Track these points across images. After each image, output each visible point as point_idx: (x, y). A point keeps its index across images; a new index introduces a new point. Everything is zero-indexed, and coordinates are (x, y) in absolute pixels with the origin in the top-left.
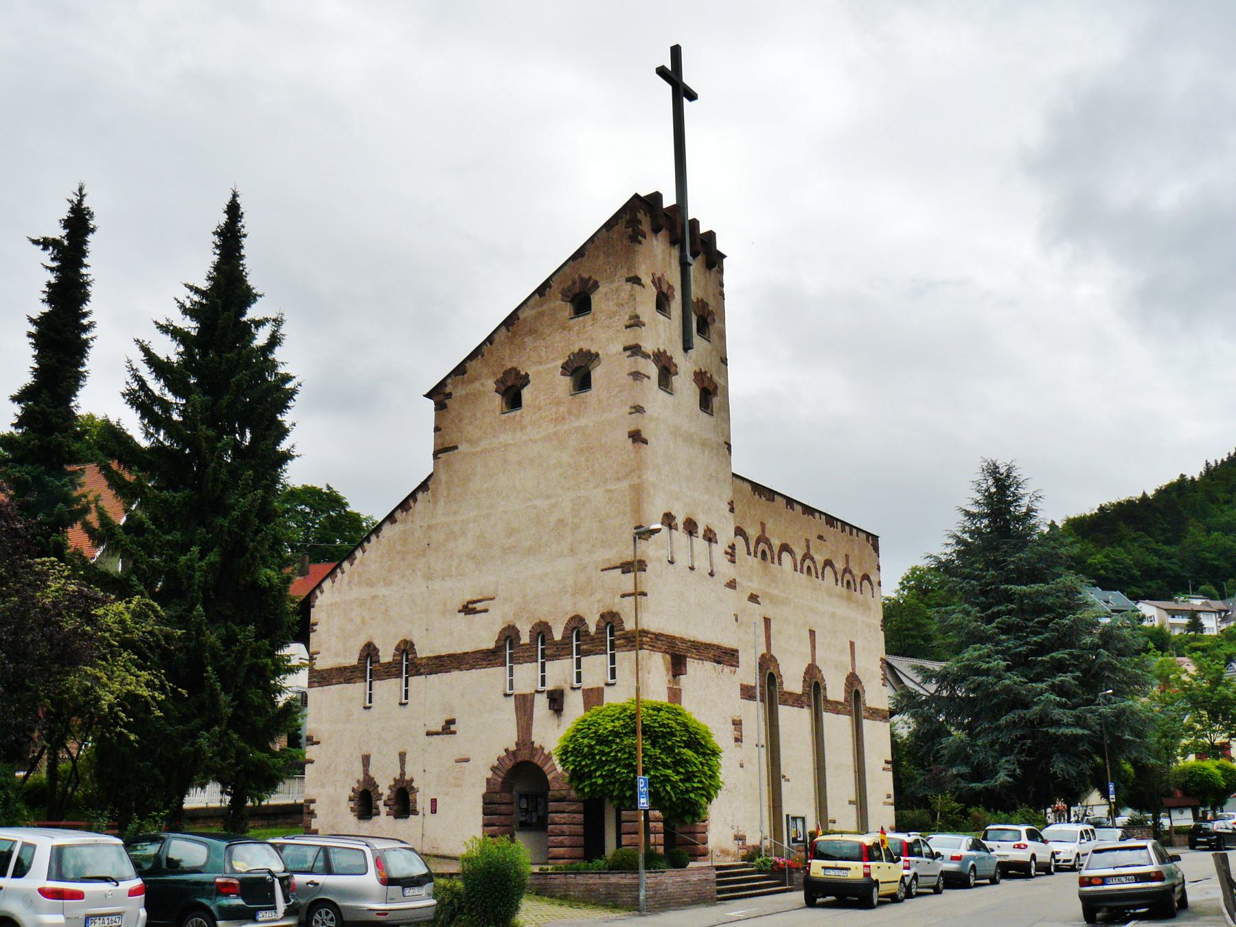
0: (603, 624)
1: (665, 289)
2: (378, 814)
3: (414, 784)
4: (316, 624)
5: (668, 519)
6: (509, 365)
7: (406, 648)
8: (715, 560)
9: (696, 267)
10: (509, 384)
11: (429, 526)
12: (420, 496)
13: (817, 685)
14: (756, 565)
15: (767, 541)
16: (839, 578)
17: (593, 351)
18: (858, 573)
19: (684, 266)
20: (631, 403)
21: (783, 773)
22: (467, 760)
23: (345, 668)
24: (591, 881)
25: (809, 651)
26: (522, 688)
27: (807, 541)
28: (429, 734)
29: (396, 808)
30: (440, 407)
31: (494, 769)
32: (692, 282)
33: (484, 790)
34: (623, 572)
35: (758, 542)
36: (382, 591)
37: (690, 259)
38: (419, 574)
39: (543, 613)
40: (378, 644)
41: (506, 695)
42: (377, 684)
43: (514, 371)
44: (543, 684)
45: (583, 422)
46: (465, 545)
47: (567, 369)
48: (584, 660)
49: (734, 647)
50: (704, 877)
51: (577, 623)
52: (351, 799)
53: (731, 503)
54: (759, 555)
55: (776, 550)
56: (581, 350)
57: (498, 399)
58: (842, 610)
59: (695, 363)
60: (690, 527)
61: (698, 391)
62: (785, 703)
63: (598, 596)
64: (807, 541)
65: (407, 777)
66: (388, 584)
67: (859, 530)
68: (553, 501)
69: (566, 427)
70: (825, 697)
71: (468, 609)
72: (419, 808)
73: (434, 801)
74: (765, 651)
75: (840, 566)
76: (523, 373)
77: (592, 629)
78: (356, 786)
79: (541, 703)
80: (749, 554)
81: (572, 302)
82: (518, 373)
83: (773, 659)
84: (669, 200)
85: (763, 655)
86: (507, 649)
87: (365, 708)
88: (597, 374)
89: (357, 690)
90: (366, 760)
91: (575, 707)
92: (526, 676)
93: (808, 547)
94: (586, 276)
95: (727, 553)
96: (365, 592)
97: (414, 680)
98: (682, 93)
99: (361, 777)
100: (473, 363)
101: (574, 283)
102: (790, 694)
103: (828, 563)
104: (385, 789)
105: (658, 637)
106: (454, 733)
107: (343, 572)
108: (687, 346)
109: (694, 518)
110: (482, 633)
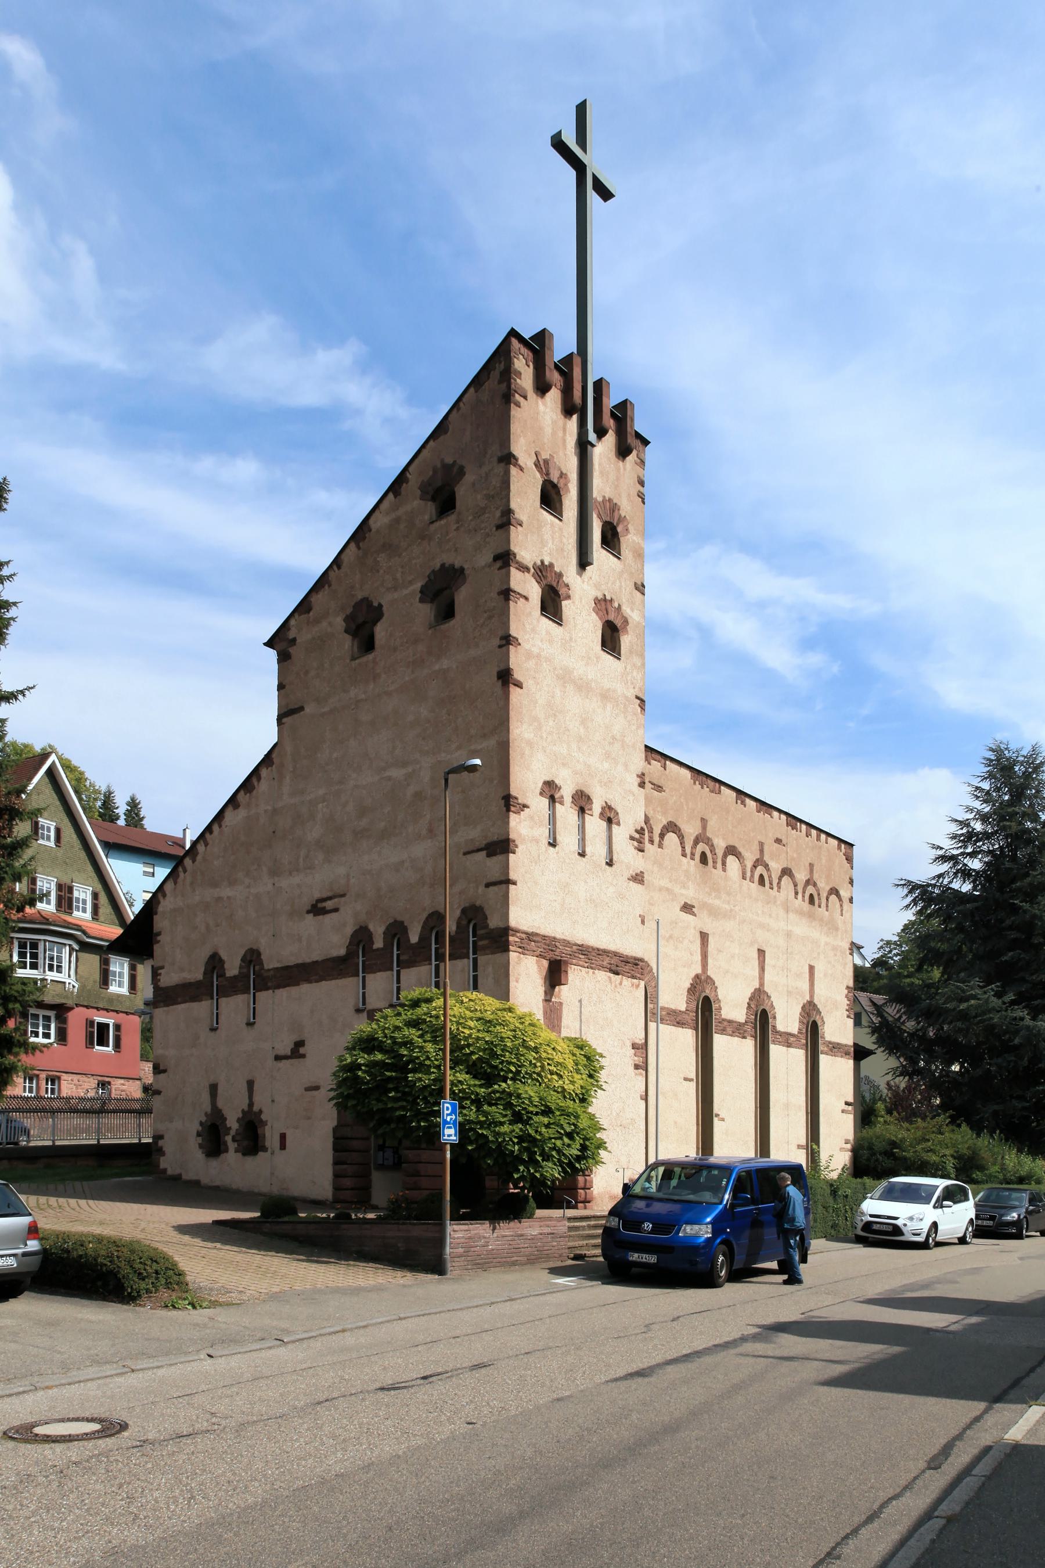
0: (464, 922)
1: (554, 477)
3: (263, 1117)
4: (159, 934)
5: (550, 791)
6: (360, 596)
7: (252, 957)
9: (603, 450)
10: (360, 620)
11: (275, 811)
12: (264, 772)
13: (764, 1013)
14: (692, 869)
15: (708, 842)
16: (800, 889)
18: (824, 886)
19: (583, 447)
20: (501, 633)
21: (716, 1110)
25: (756, 973)
27: (761, 845)
28: (278, 1058)
29: (245, 1143)
30: (284, 658)
33: (335, 1123)
34: (489, 855)
35: (696, 842)
36: (226, 892)
37: (592, 437)
38: (264, 869)
40: (224, 957)
43: (366, 602)
45: (445, 663)
46: (314, 832)
50: (547, 1230)
52: (199, 1134)
54: (697, 857)
55: (720, 853)
56: (443, 565)
57: (347, 641)
58: (801, 928)
59: (597, 586)
60: (582, 802)
61: (599, 625)
62: (723, 1031)
64: (761, 845)
65: (256, 1109)
66: (232, 883)
67: (828, 835)
70: (774, 1027)
71: (317, 909)
72: (267, 1144)
73: (283, 1137)
74: (699, 971)
75: (801, 876)
76: (376, 604)
78: (204, 1119)
80: (684, 855)
81: (433, 499)
83: (710, 980)
84: (564, 344)
85: (697, 976)
86: (359, 956)
89: (202, 1009)
90: (214, 1089)
93: (762, 851)
94: (449, 460)
95: (632, 838)
97: (262, 996)
98: (590, 187)
101: (435, 471)
102: (730, 1022)
103: (786, 872)
104: (233, 1123)
105: (531, 936)
107: (185, 871)
108: (584, 562)
109: (587, 791)
110: (330, 938)
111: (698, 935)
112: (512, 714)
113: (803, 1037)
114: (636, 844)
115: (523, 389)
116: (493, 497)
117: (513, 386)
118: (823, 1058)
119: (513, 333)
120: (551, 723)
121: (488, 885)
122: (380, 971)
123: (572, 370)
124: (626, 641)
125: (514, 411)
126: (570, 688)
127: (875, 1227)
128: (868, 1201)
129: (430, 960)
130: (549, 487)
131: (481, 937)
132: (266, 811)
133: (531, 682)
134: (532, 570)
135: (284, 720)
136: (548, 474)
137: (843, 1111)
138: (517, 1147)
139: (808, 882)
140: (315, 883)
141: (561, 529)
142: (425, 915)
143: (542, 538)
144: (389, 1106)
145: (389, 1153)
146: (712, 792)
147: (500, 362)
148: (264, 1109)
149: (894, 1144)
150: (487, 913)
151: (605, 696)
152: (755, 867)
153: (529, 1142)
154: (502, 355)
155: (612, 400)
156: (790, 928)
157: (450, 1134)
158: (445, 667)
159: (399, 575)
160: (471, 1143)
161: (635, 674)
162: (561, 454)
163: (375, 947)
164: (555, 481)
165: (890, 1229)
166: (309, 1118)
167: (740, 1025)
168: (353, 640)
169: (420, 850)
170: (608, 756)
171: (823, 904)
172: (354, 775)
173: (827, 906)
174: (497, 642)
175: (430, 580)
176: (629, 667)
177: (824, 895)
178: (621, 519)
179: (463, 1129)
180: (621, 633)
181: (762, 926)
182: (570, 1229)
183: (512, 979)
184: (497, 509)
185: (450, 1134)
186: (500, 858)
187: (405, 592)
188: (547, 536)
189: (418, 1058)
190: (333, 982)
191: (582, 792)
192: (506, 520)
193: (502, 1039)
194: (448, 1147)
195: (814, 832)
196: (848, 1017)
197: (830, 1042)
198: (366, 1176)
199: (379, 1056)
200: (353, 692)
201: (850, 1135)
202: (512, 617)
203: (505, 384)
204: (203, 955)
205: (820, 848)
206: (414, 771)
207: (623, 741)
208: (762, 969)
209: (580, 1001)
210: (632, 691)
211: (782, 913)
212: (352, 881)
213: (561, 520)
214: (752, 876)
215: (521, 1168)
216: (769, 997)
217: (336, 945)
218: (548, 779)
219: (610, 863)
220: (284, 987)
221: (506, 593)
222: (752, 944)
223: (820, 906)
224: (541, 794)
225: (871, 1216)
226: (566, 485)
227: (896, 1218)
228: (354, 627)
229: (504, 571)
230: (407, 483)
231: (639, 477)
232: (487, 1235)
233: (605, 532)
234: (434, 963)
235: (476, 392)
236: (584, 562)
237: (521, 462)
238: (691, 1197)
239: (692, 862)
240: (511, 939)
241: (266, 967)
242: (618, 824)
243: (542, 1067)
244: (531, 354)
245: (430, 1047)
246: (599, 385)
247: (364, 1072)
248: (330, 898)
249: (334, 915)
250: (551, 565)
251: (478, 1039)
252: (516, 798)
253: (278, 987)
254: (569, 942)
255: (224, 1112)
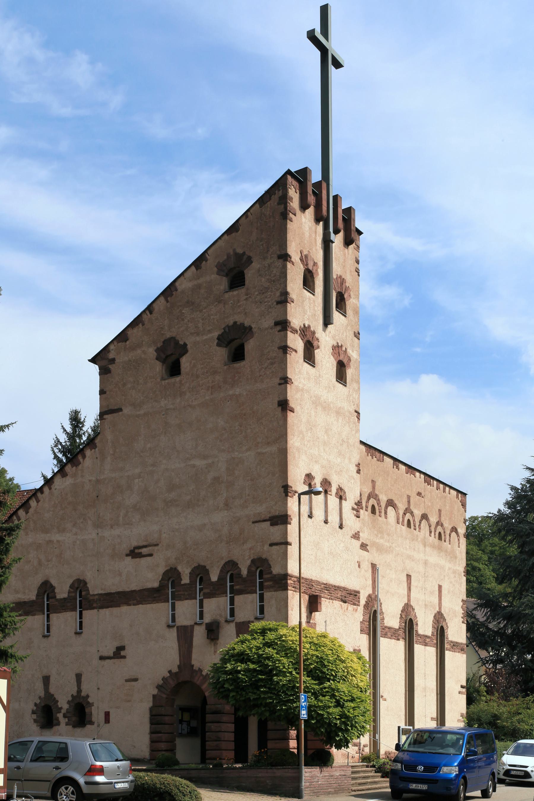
2: (58, 724)
3: (90, 700)
6: (168, 335)
7: (79, 586)
8: (344, 516)
9: (338, 240)
10: (169, 353)
11: (98, 481)
13: (442, 628)
14: (367, 518)
15: (376, 497)
16: (433, 530)
17: (247, 324)
18: (448, 526)
19: (327, 243)
20: (281, 375)
22: (136, 680)
23: (25, 603)
24: (260, 775)
25: (406, 592)
26: (183, 620)
27: (409, 497)
28: (102, 658)
29: (74, 719)
30: (104, 372)
31: (159, 687)
32: (334, 259)
33: (151, 704)
34: (272, 525)
35: (369, 498)
36: (56, 537)
38: (90, 522)
39: (201, 557)
40: (54, 582)
41: (169, 626)
42: (54, 617)
44: (201, 617)
45: (237, 391)
47: (223, 340)
48: (237, 598)
49: (357, 589)
50: (343, 773)
51: (231, 566)
52: (33, 712)
53: (358, 465)
55: (383, 505)
56: (235, 323)
58: (434, 558)
59: (333, 338)
61: (335, 363)
62: (385, 636)
63: (248, 545)
64: (409, 497)
65: (83, 694)
66: (62, 531)
67: (451, 487)
68: (210, 461)
69: (222, 395)
71: (135, 553)
73: (107, 715)
74: (371, 592)
75: (433, 519)
76: (181, 343)
77: (244, 572)
78: (38, 701)
79: (199, 634)
81: (227, 275)
82: (177, 343)
84: (316, 176)
85: (369, 596)
86: (169, 588)
87: (44, 636)
88: (250, 346)
90: (46, 680)
91: (229, 640)
92: (186, 612)
93: (409, 502)
94: (240, 251)
95: (353, 509)
96: (41, 537)
99: (42, 694)
100: (135, 330)
101: (229, 256)
102: (389, 628)
103: (424, 517)
104: (63, 703)
106: (124, 657)
108: (327, 321)
110: (146, 574)
111: (370, 566)
112: (289, 430)
113: (434, 638)
114: (355, 512)
115: (294, 209)
116: (274, 281)
117: (288, 208)
118: (447, 653)
119: (289, 172)
120: (309, 434)
121: (271, 545)
122: (187, 599)
123: (322, 192)
124: (350, 372)
125: (290, 226)
126: (319, 408)
127: (513, 773)
128: (505, 756)
129: (227, 593)
130: (307, 273)
131: (267, 578)
132: (90, 481)
133: (298, 407)
134: (299, 332)
135: (105, 417)
136: (307, 265)
137: (460, 693)
138: (338, 722)
139: (438, 523)
140: (136, 533)
141: (314, 301)
142: (223, 562)
143: (304, 308)
144: (262, 696)
145: (185, 726)
146: (378, 460)
147: (279, 190)
148: (90, 694)
149: (496, 717)
150: (271, 563)
151: (338, 412)
152: (405, 514)
153: (345, 718)
154: (280, 185)
155: (344, 205)
156: (427, 558)
157: (304, 714)
158: (237, 393)
159: (200, 325)
160: (313, 719)
161: (354, 395)
162: (314, 249)
163: (183, 582)
164: (311, 268)
165: (522, 774)
166: (129, 701)
167: (396, 630)
168: (163, 365)
169: (219, 517)
170: (340, 454)
171: (447, 540)
172: (164, 461)
173: (450, 541)
174: (278, 381)
175: (225, 331)
176: (351, 391)
177: (448, 532)
178: (347, 289)
179: (310, 709)
180: (347, 368)
181: (410, 558)
182: (353, 772)
183: (289, 608)
184: (277, 290)
185: (304, 714)
186: (281, 527)
187: (205, 337)
188: (307, 308)
189: (279, 667)
190: (148, 605)
191: (326, 479)
192: (284, 299)
193: (327, 655)
194: (303, 721)
195: (441, 486)
196: (463, 622)
197: (452, 642)
198: (172, 741)
199: (252, 666)
200: (163, 403)
201: (464, 711)
202: (288, 365)
203: (283, 206)
204: (36, 582)
205: (445, 497)
206: (213, 462)
207: (348, 442)
208: (409, 589)
209: (325, 622)
210: (353, 407)
211: (421, 547)
212: (164, 535)
213: (314, 295)
214: (403, 521)
215: (340, 734)
216: (413, 609)
217: (152, 580)
218: (308, 472)
219: (341, 527)
220: (107, 607)
221: (285, 349)
222: (403, 571)
223: (445, 541)
224: (304, 483)
225: (510, 765)
226: (317, 270)
227: (527, 767)
228: (163, 356)
229: (282, 333)
230: (206, 261)
231: (356, 258)
232: (318, 775)
233: (336, 300)
234: (229, 595)
235: (260, 207)
236: (327, 321)
237: (293, 259)
238: (441, 751)
239: (366, 513)
240: (289, 582)
241: (91, 593)
242: (346, 500)
243: (348, 672)
244: (298, 184)
245: (285, 660)
246: (336, 198)
247: (243, 675)
248: (145, 546)
249: (149, 559)
250: (309, 327)
251: (312, 655)
252: (291, 487)
253: (102, 607)
254: (319, 582)
255: (55, 696)
